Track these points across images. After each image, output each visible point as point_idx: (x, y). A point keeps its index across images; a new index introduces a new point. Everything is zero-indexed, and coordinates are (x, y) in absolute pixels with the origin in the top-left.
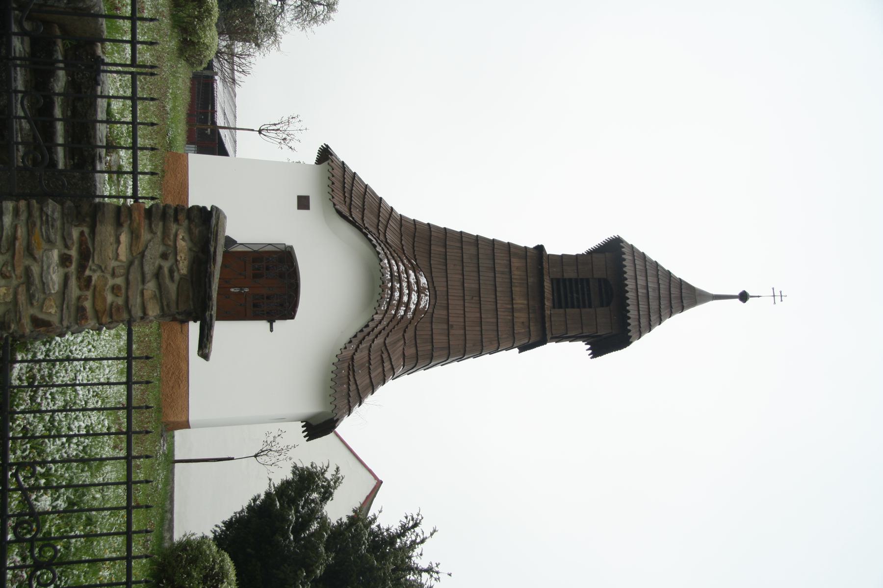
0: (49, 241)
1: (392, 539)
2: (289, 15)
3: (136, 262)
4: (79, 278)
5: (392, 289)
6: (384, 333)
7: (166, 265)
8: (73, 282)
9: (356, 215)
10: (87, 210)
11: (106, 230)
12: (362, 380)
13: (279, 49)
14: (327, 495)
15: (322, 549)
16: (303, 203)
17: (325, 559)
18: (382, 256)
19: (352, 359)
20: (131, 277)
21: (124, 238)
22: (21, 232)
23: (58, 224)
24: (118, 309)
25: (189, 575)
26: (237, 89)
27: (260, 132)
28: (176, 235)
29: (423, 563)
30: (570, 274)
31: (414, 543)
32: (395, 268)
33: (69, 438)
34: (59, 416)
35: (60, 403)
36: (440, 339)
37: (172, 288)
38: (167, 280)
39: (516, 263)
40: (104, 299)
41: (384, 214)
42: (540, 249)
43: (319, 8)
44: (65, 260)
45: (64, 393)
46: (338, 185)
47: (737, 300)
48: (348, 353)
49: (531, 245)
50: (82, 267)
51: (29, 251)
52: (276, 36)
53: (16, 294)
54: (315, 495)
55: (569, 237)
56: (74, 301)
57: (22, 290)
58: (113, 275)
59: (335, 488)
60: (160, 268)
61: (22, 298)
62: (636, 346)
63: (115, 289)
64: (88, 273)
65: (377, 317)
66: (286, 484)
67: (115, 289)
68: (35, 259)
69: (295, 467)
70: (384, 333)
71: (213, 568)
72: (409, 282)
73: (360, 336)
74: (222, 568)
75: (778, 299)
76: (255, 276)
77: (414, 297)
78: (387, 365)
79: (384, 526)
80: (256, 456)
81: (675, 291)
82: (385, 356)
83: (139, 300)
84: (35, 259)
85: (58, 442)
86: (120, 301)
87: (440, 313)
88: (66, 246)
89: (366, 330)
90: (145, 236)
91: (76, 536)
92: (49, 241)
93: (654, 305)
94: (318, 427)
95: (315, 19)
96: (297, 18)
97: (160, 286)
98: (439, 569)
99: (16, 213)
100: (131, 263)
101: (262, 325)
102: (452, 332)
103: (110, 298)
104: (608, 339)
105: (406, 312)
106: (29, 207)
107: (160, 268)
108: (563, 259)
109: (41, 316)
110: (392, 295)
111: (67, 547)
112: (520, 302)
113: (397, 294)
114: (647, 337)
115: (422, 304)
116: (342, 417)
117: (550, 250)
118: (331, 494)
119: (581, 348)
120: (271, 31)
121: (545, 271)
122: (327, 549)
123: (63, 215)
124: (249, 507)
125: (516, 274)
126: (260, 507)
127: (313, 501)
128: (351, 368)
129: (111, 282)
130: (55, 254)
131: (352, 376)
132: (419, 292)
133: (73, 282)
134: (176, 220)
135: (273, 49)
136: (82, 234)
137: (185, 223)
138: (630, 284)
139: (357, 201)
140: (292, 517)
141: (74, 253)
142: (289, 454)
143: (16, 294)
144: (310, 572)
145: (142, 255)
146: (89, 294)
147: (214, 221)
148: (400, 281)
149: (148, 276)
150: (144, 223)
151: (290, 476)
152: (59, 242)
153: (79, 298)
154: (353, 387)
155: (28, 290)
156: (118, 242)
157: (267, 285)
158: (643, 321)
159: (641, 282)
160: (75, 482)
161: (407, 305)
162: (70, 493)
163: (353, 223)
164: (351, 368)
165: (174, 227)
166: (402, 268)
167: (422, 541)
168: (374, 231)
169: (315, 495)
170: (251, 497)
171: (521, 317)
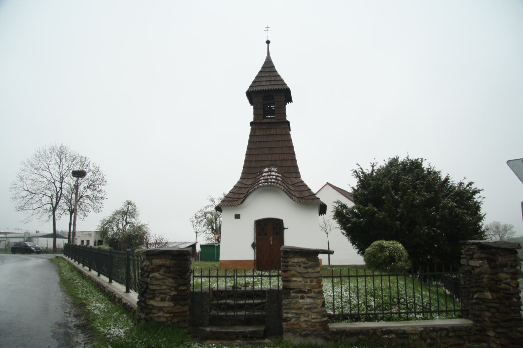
0: (296, 303)
1: (361, 181)
2: (133, 220)
3: (302, 275)
4: (308, 293)
5: (271, 182)
6: (288, 185)
7: (303, 265)
8: (309, 295)
9: (242, 196)
10: (286, 291)
11: (292, 285)
12: (307, 194)
13: (147, 225)
14: (344, 206)
15: (367, 208)
16: (237, 217)
17: (370, 207)
18: (258, 186)
19: (298, 198)
20: (308, 276)
21: (294, 279)
22: (294, 311)
23: (290, 300)
24: (318, 280)
25: (379, 257)
26: (169, 241)
27: (197, 233)
28: (293, 262)
29: (370, 169)
30: (261, 112)
31: (363, 172)
32: (263, 181)
33: (350, 297)
34: (344, 300)
35: (339, 300)
36: (289, 163)
37: (310, 263)
38: (308, 265)
39: (257, 133)
40: (315, 285)
41: (240, 185)
42: (251, 124)
43: (130, 208)
44: (302, 298)
45: (336, 299)
46: (230, 203)
47: (269, 45)
48: (296, 199)
49: (250, 127)
50: (304, 292)
51: (300, 309)
52: (142, 226)
53: (314, 312)
54: (344, 211)
55: (247, 113)
56: (316, 295)
57: (312, 311)
58: (307, 282)
59: (342, 203)
60: (304, 267)
61: (316, 310)
62: (289, 86)
63: (311, 282)
64: (306, 290)
65: (283, 188)
66: (340, 222)
67: (311, 282)
68: (302, 307)
69: (334, 219)
70: (288, 185)
71: (377, 249)
72: (268, 176)
73: (290, 195)
74: (377, 246)
75: (269, 29)
76: (266, 234)
77: (273, 173)
78: (300, 184)
79: (356, 184)
80: (327, 234)
81: (267, 70)
82: (296, 185)
83: (315, 274)
84: (302, 307)
85: (352, 300)
86: (315, 280)
87: (278, 163)
88: (298, 297)
89: (288, 192)
90: (293, 272)
91: (382, 293)
92: (296, 303)
93: (273, 78)
94: (323, 209)
95: (135, 210)
96: (134, 217)
97: (310, 267)
98: (372, 163)
99: (287, 313)
100: (303, 277)
101: (286, 232)
102: (286, 159)
103: (314, 283)
104: (286, 95)
105: (279, 177)
106: (285, 309)
107: (304, 267)
108: (255, 114)
109: (321, 305)
110: (274, 182)
111: (385, 296)
112: (273, 132)
113: (273, 180)
114: (286, 81)
115: (275, 170)
116: (321, 201)
117: (252, 120)
118: (344, 205)
119: (288, 106)
120: (140, 228)
121: (261, 121)
122: (367, 206)
123: (287, 298)
124: (347, 235)
125: (261, 133)
126: (346, 231)
127: (346, 212)
128: (302, 198)
129: (309, 283)
130: (301, 301)
131: (305, 198)
132: (271, 171)
133: (309, 295)
134: (288, 262)
135: (147, 227)
136: (293, 292)
137: (288, 259)
138: (265, 88)
139: (237, 196)
140: (354, 220)
141: (300, 295)
142: (326, 221)
143: (314, 312)
144: (376, 213)
145: (300, 273)
146: (313, 290)
147: (288, 250)
148: (267, 179)
149: (307, 271)
150: (289, 273)
151: (337, 220)
152: (296, 300)
153: (315, 293)
154: (309, 197)
155: (312, 309)
156: (296, 281)
157: (269, 231)
158: (280, 83)
159: (264, 83)
160: (365, 294)
161: (276, 176)
162: (369, 297)
163: (246, 197)
164: (302, 198)
165: (290, 263)
166: (262, 178)
167: (362, 169)
168: (248, 189)
169: (344, 211)
170: (342, 235)
171: (279, 131)
